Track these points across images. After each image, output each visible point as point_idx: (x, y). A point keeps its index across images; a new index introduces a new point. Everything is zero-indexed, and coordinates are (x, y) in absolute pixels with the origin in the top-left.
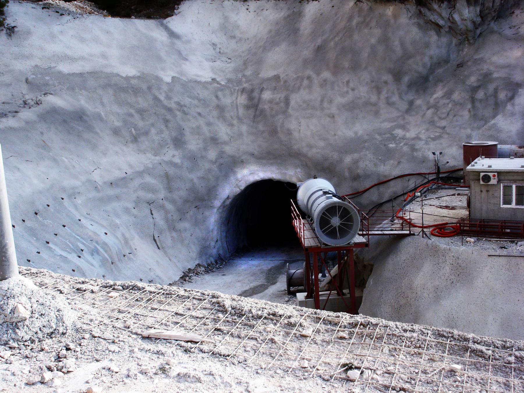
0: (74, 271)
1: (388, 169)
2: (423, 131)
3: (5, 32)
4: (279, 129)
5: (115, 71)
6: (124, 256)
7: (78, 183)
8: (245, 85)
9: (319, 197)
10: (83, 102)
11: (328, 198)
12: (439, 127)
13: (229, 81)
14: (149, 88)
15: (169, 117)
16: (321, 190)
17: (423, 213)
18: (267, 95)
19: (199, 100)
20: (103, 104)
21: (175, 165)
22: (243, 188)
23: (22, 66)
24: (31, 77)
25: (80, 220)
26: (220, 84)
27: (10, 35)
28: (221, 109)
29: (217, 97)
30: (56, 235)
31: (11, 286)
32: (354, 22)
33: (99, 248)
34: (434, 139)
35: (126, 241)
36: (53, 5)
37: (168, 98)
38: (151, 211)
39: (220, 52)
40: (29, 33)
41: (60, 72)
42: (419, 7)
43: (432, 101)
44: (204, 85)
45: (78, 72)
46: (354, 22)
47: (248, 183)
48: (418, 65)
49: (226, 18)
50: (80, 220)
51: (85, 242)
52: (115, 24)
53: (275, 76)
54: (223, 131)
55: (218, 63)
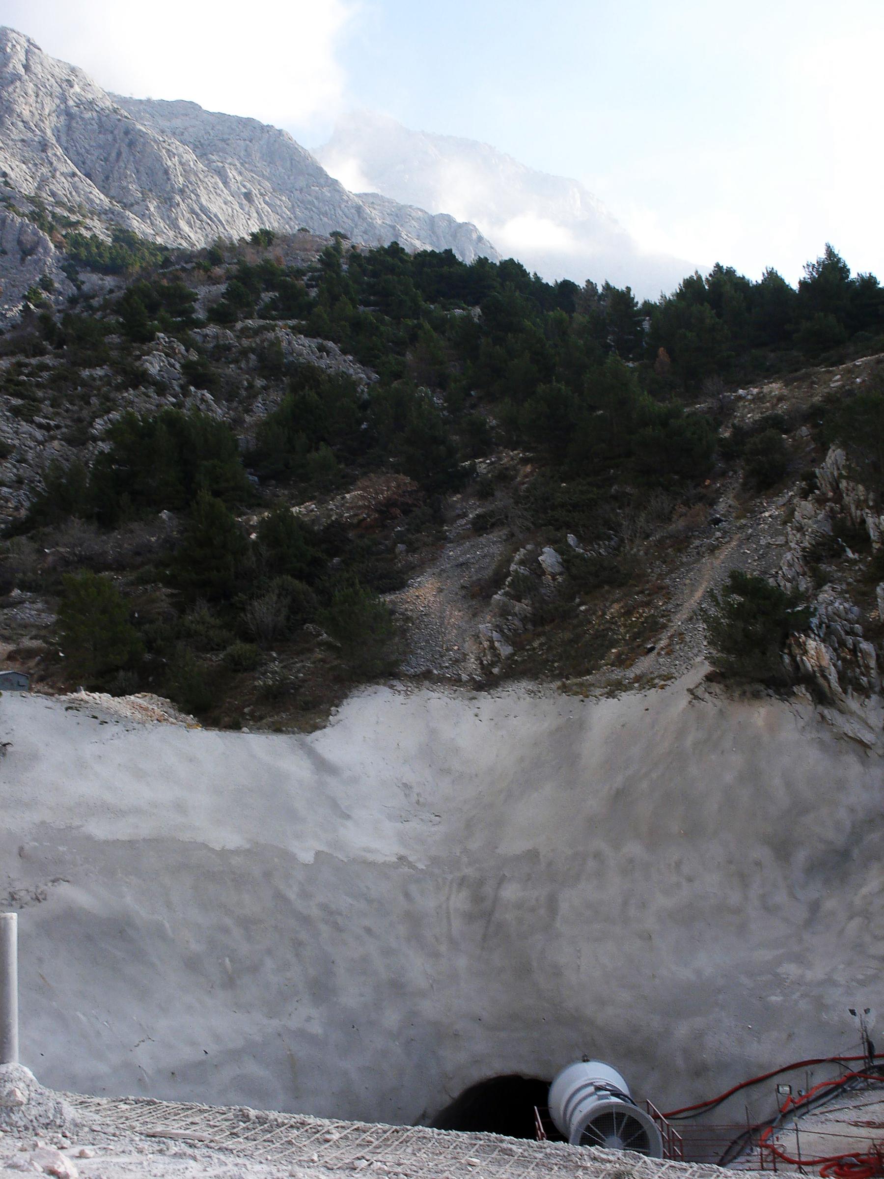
1: (768, 1051)
2: (842, 966)
4: (535, 964)
5: (200, 839)
7: (103, 1068)
8: (468, 871)
10: (129, 900)
11: (601, 1098)
12: (874, 957)
13: (435, 861)
14: (267, 875)
15: (303, 936)
16: (591, 1084)
18: (511, 892)
19: (370, 901)
20: (169, 905)
21: (312, 1040)
22: (456, 1094)
23: (19, 823)
24: (30, 845)
26: (414, 868)
28: (414, 920)
29: (407, 895)
31: (10, 1070)
32: (689, 741)
34: (862, 983)
37: (305, 895)
39: (418, 802)
40: (34, 757)
41: (89, 838)
42: (820, 708)
43: (858, 901)
44: (382, 869)
45: (126, 838)
46: (689, 741)
48: (827, 826)
49: (433, 733)
52: (207, 744)
54: (417, 968)
55: (414, 825)
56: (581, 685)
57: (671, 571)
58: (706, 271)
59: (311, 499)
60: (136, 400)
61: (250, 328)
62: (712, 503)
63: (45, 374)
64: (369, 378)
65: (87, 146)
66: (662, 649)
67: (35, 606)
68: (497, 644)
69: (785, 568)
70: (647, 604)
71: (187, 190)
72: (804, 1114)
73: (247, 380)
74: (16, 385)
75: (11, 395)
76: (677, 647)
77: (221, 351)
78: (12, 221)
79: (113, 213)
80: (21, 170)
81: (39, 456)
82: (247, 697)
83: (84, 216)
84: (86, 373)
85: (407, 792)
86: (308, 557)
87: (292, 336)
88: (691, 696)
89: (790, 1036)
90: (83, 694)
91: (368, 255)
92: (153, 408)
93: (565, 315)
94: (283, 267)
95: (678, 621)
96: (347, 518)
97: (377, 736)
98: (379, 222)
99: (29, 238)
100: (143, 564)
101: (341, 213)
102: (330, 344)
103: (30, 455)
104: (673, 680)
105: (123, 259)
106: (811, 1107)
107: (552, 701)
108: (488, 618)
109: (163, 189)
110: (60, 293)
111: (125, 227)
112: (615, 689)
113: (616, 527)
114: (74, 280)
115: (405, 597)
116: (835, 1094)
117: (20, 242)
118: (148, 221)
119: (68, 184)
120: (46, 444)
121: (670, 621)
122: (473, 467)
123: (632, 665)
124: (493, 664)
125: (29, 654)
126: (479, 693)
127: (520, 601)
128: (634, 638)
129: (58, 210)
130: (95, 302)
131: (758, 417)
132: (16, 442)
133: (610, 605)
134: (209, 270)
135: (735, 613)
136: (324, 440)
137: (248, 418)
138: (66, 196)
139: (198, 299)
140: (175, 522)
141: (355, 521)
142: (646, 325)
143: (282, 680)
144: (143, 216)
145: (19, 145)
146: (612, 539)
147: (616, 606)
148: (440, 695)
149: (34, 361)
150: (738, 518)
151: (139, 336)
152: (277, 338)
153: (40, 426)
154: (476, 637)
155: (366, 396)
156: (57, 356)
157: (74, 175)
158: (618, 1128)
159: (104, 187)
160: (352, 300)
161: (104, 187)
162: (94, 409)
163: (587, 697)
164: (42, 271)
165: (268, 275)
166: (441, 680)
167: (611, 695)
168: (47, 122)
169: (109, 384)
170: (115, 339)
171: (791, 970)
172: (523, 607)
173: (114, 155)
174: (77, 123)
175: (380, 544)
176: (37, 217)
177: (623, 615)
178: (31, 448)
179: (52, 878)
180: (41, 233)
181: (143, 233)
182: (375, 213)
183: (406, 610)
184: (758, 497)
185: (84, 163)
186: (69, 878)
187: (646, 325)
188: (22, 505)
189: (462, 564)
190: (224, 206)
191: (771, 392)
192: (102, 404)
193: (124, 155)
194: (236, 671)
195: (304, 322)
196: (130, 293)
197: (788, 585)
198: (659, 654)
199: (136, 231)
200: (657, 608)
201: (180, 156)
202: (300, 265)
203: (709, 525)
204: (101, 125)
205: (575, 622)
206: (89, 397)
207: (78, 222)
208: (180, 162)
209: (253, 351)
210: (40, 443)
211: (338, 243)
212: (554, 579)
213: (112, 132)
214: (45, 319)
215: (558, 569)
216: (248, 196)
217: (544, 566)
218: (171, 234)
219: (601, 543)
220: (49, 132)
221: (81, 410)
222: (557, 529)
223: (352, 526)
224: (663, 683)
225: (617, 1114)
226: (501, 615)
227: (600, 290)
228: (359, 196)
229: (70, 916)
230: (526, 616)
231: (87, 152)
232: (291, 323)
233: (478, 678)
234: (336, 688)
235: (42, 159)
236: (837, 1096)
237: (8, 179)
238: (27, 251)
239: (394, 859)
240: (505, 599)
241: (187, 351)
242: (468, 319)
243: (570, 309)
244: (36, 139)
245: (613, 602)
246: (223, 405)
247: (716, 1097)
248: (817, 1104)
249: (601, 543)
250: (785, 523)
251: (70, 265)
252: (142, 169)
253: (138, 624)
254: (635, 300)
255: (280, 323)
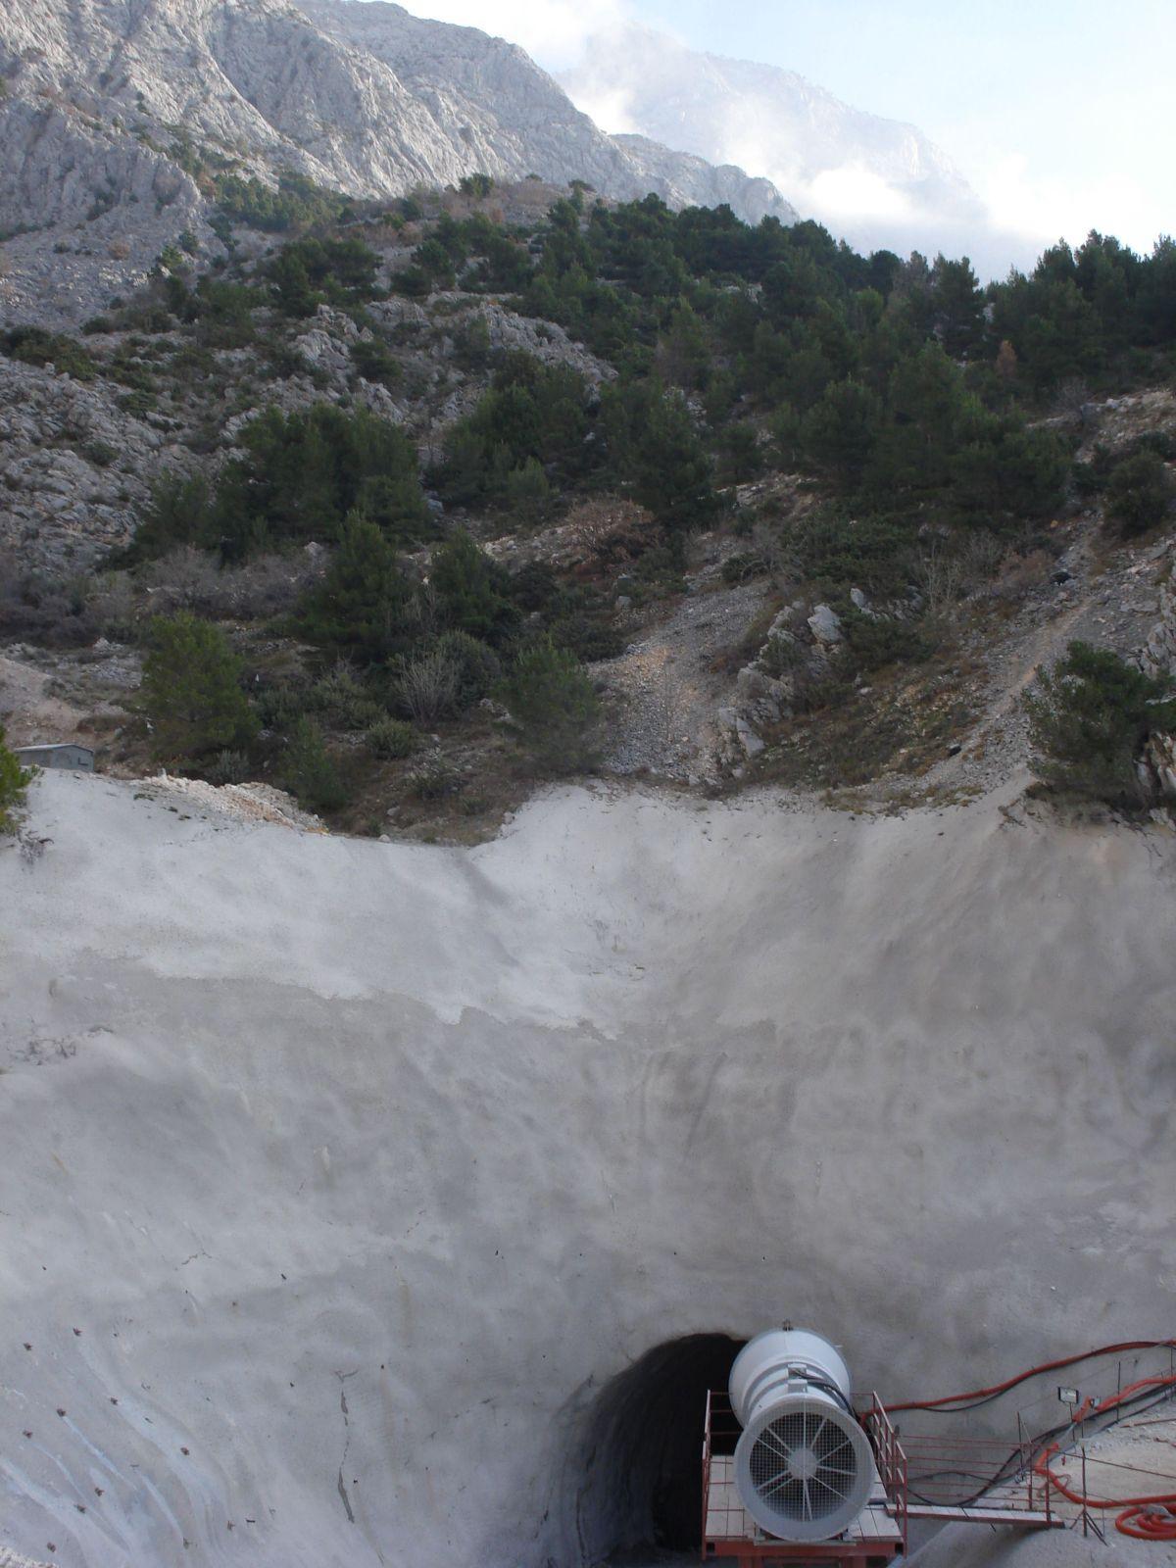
0: (52, 1548)
1: (1077, 1325)
3: (17, 850)
6: (230, 1526)
9: (772, 1386)
11: (793, 1389)
16: (785, 1365)
17: (1084, 1458)
25: (114, 1402)
27: (30, 862)
29: (587, 1075)
30: (29, 1435)
33: (153, 1490)
35: (246, 1482)
36: (166, 789)
38: (344, 1399)
39: (615, 949)
45: (197, 976)
47: (655, 1341)
50: (114, 1402)
51: (113, 1469)
52: (326, 855)
53: (762, 1022)
54: (593, 1177)
56: (854, 796)
57: (992, 644)
58: (1077, 242)
59: (510, 533)
60: (286, 394)
61: (448, 303)
62: (1057, 553)
63: (167, 356)
64: (604, 375)
65: (251, 61)
66: (970, 750)
67: (126, 662)
68: (741, 736)
69: (1152, 644)
70: (955, 688)
71: (383, 123)
72: (1110, 1425)
73: (438, 371)
74: (127, 369)
75: (119, 381)
76: (992, 749)
77: (406, 333)
78: (146, 157)
79: (283, 152)
80: (162, 90)
81: (152, 464)
82: (393, 795)
83: (244, 155)
84: (221, 356)
85: (601, 933)
86: (495, 612)
87: (502, 315)
88: (1004, 818)
89: (1109, 1305)
90: (164, 779)
91: (616, 210)
92: (309, 405)
93: (877, 296)
94: (501, 224)
95: (996, 713)
96: (555, 559)
97: (562, 850)
98: (642, 173)
99: (168, 181)
100: (276, 611)
101: (590, 160)
102: (554, 327)
103: (140, 464)
104: (981, 794)
105: (292, 212)
106: (1123, 1412)
107: (811, 817)
108: (733, 699)
109: (351, 121)
110: (206, 256)
111: (298, 170)
112: (900, 803)
113: (920, 582)
114: (225, 239)
115: (621, 668)
116: (1163, 1395)
117: (155, 186)
118: (330, 164)
119: (228, 114)
120: (162, 449)
121: (984, 712)
122: (732, 497)
123: (926, 772)
124: (734, 763)
125: (107, 724)
126: (711, 802)
127: (778, 678)
128: (933, 735)
129: (210, 146)
130: (248, 267)
131: (1130, 435)
132: (122, 445)
133: (903, 689)
134: (401, 226)
135: (1074, 702)
136: (534, 454)
137: (435, 423)
138: (221, 127)
139: (382, 264)
140: (324, 557)
141: (566, 564)
142: (988, 312)
143: (441, 773)
144: (323, 157)
145: (161, 56)
146: (914, 598)
147: (911, 690)
148: (657, 803)
149: (154, 338)
150: (1092, 574)
151: (296, 308)
152: (481, 316)
153: (155, 425)
154: (714, 725)
155: (595, 397)
156: (184, 333)
157: (233, 99)
158: (809, 1440)
159: (272, 116)
160: (587, 268)
161: (272, 116)
162: (230, 404)
163: (860, 813)
164: (183, 226)
165: (478, 235)
166: (660, 782)
167: (892, 811)
168: (199, 28)
169: (251, 371)
170: (265, 312)
171: (1119, 1211)
172: (782, 686)
173: (287, 72)
174: (240, 29)
175: (596, 595)
176: (180, 153)
177: (920, 702)
178: (141, 454)
179: (91, 1025)
180: (184, 174)
181: (323, 179)
182: (637, 162)
183: (622, 685)
184: (1123, 547)
185: (247, 84)
186: (115, 1027)
187: (988, 312)
188: (125, 530)
189: (703, 626)
190: (432, 146)
191: (1153, 403)
192: (240, 397)
193: (300, 74)
194: (380, 758)
195: (521, 297)
196: (287, 250)
197: (1155, 668)
198: (965, 758)
199: (314, 177)
200: (967, 694)
201: (376, 77)
202: (523, 222)
203: (1052, 582)
204: (271, 34)
205: (852, 709)
206: (224, 389)
207: (235, 162)
208: (376, 85)
209: (449, 333)
210: (154, 447)
211: (578, 195)
212: (828, 649)
213: (286, 43)
214: (173, 285)
215: (834, 635)
216: (466, 134)
217: (814, 630)
218: (360, 181)
219: (898, 602)
220: (201, 39)
221: (212, 405)
222: (838, 581)
223: (560, 571)
224: (966, 798)
225: (809, 1416)
226: (750, 697)
227: (931, 265)
228: (616, 137)
229: (107, 1078)
230: (785, 699)
231: (252, 69)
232: (503, 297)
233: (712, 782)
234: (514, 786)
235: (191, 76)
236: (1165, 1399)
237: (144, 102)
238: (164, 198)
239: (573, 1024)
240: (757, 674)
241: (359, 330)
242: (742, 297)
243: (885, 288)
244: (184, 49)
245: (907, 684)
246: (404, 405)
247: (997, 1384)
248: (1131, 1409)
249: (898, 602)
250: (1157, 583)
251: (221, 219)
252: (324, 93)
253: (251, 688)
254: (975, 277)
255: (489, 297)
